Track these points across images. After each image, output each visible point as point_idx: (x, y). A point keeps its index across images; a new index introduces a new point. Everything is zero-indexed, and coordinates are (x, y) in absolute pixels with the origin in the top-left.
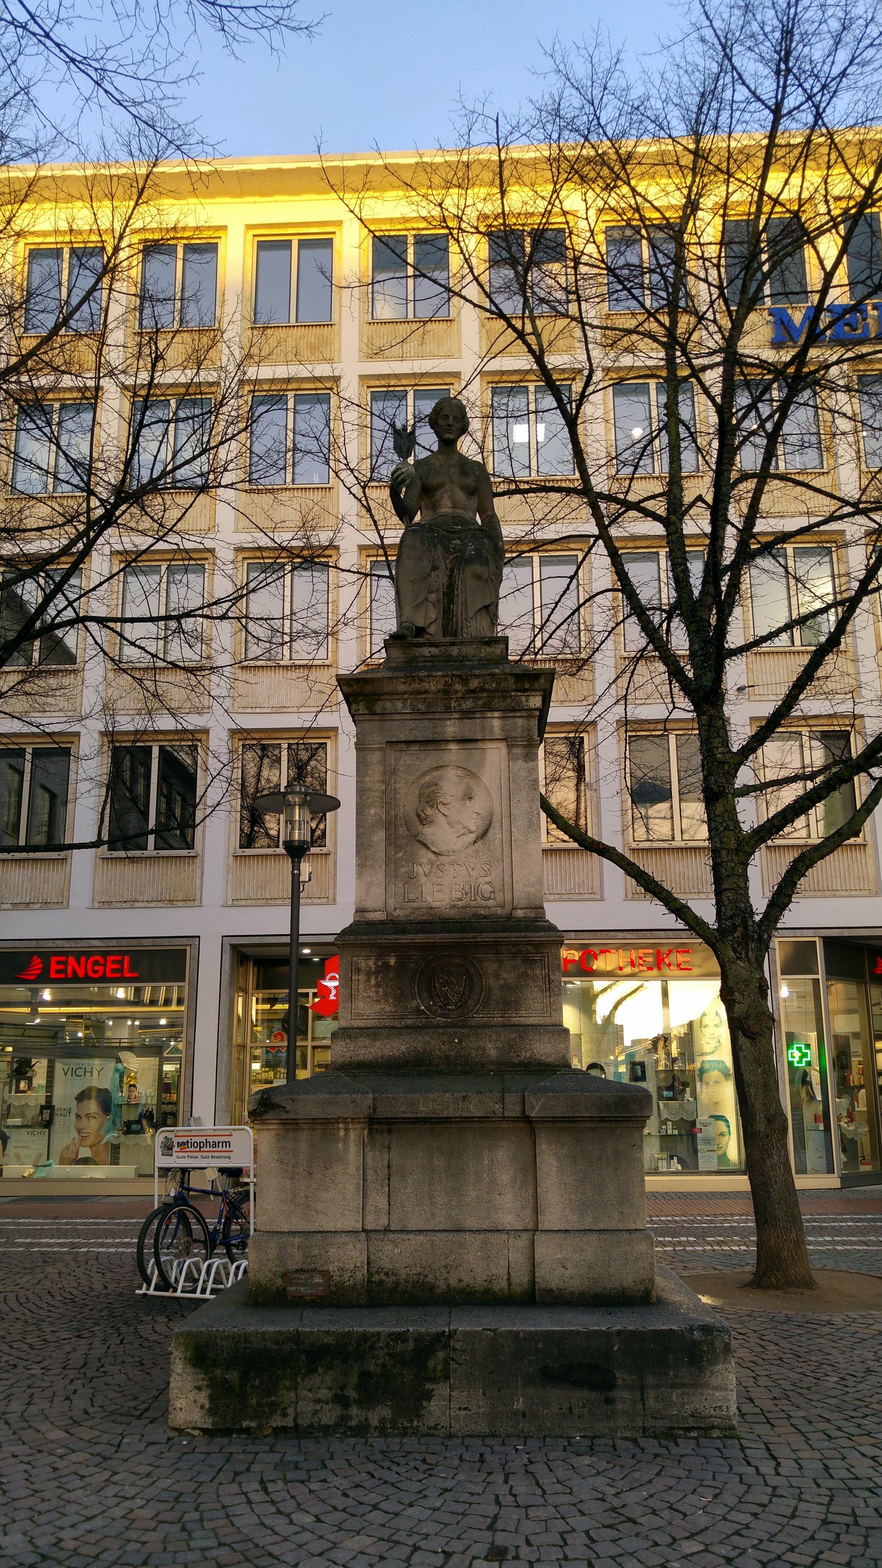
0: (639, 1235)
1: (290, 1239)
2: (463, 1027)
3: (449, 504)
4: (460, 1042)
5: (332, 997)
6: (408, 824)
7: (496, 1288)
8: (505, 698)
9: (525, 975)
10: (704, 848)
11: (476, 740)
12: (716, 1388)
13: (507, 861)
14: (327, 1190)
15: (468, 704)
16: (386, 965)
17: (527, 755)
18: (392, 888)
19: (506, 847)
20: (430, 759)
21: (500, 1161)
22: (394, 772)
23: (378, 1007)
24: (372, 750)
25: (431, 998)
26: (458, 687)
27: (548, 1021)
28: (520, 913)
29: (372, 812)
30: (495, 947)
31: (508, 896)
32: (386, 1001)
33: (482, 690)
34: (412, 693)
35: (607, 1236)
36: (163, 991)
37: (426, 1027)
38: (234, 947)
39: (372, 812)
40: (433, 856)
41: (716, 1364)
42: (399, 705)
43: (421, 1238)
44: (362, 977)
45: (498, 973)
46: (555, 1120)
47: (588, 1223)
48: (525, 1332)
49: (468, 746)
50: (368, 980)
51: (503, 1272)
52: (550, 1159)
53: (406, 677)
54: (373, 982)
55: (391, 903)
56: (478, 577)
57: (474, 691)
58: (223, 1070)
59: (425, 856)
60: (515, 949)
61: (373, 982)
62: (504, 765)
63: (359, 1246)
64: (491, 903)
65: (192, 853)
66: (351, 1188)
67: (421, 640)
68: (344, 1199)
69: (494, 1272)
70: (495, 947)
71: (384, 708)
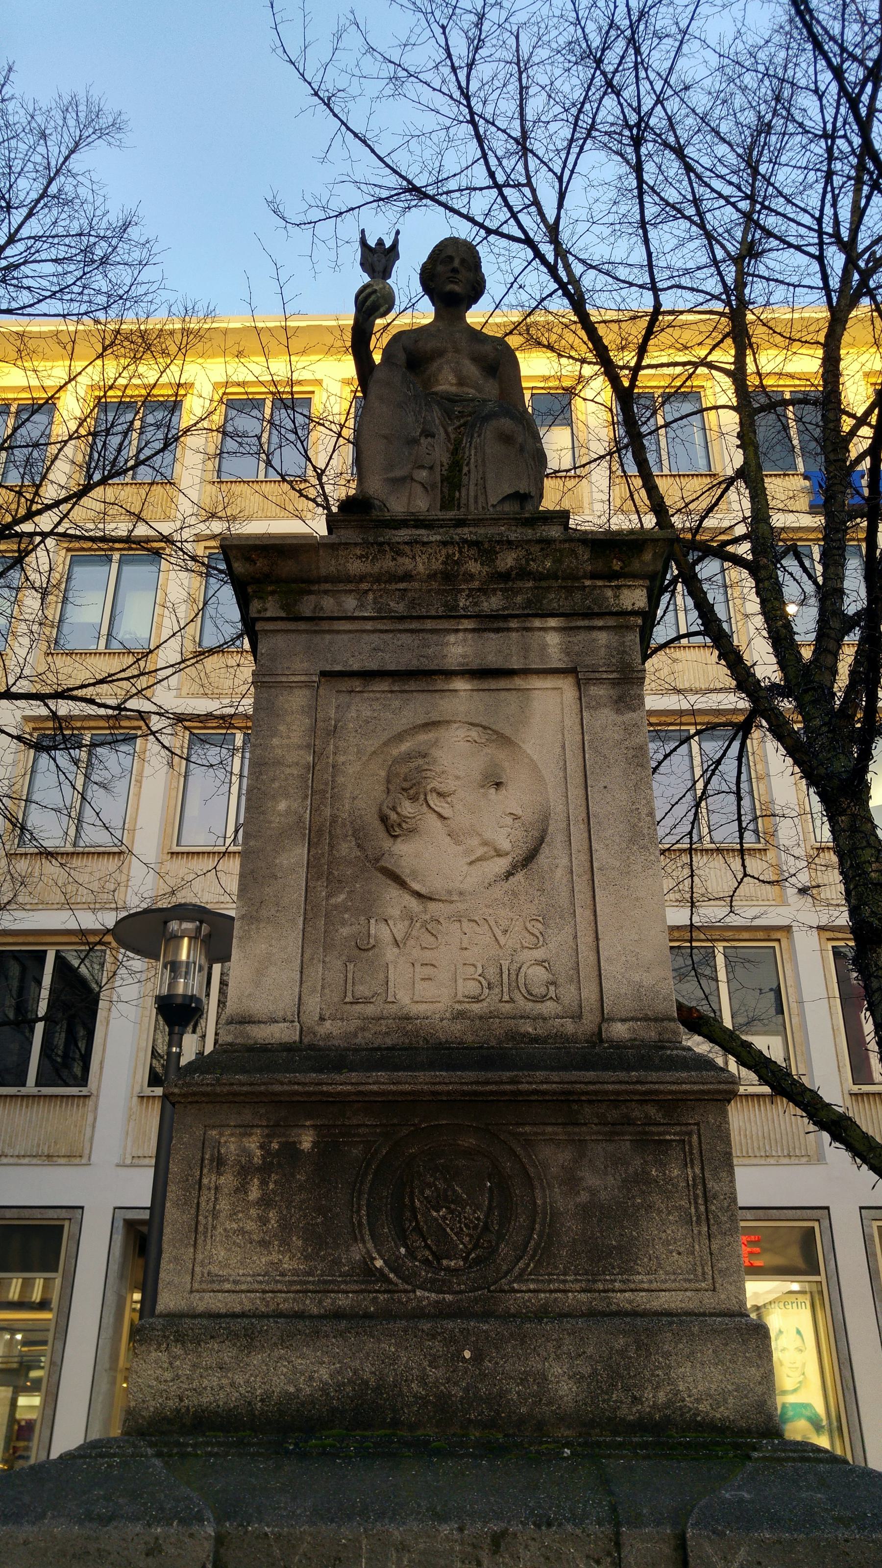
2: (486, 1316)
3: (452, 378)
4: (478, 1358)
6: (360, 836)
8: (570, 590)
9: (642, 1180)
11: (510, 673)
13: (583, 915)
15: (493, 603)
16: (291, 1150)
18: (316, 972)
19: (582, 885)
20: (412, 709)
22: (334, 732)
23: (261, 1261)
24: (290, 687)
25: (402, 1237)
26: (473, 567)
27: (709, 1301)
28: (619, 1030)
29: (282, 806)
30: (565, 1106)
31: (589, 993)
32: (285, 1243)
34: (377, 579)
36: (39, 1284)
37: (387, 1315)
39: (282, 806)
40: (414, 904)
42: (350, 603)
44: (228, 1180)
45: (573, 1176)
49: (493, 684)
50: (242, 1189)
53: (366, 544)
54: (254, 1194)
55: (313, 1005)
57: (505, 576)
58: (98, 1407)
59: (395, 901)
60: (614, 1115)
61: (254, 1194)
62: (571, 721)
64: (548, 1008)
65: (84, 1091)
70: (565, 1106)
71: (318, 607)
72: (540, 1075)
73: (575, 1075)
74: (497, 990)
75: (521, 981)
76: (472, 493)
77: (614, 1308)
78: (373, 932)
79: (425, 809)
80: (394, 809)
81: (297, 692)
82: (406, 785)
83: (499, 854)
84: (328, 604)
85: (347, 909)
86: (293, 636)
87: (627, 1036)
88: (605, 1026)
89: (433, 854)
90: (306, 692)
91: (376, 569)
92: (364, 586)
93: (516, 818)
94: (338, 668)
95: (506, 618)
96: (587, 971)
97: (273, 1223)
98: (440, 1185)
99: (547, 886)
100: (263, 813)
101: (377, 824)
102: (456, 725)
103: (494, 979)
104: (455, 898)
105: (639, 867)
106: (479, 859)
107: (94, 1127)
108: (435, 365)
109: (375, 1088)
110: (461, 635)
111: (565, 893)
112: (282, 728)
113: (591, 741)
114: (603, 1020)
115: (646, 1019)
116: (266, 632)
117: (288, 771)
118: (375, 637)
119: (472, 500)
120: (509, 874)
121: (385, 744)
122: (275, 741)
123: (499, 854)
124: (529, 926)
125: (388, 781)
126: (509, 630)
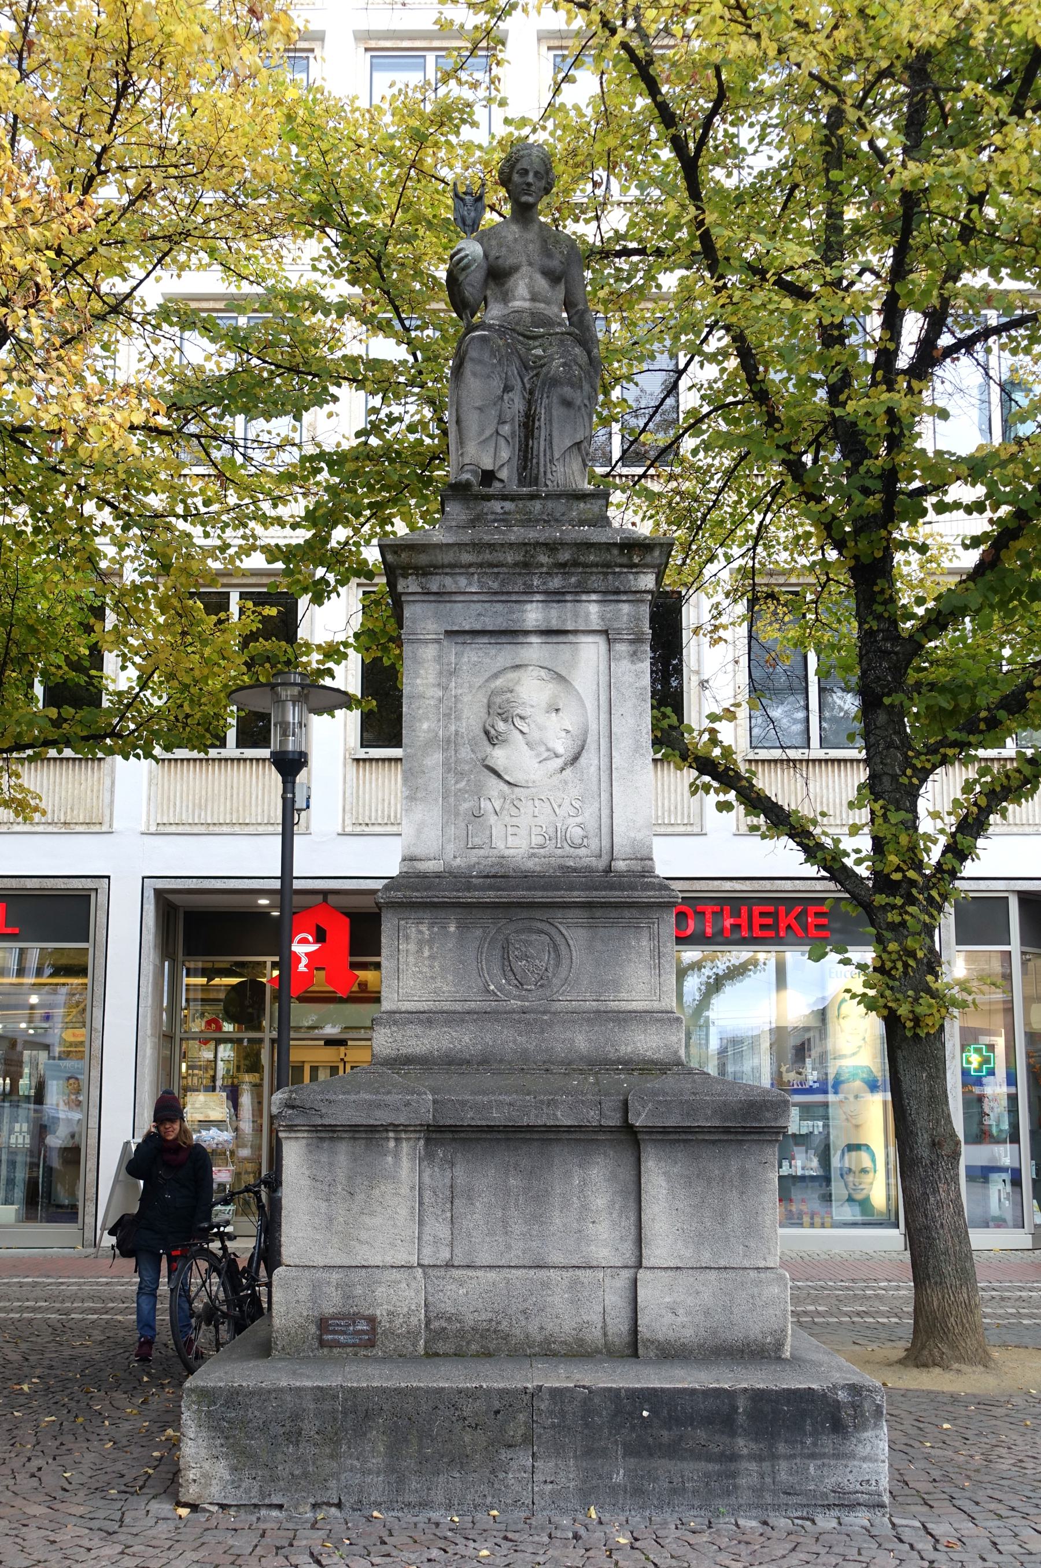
0: (769, 1274)
1: (325, 1275)
5: (302, 968)
7: (588, 1338)
10: (858, 761)
12: (864, 1459)
13: (605, 796)
14: (372, 1214)
15: (556, 583)
17: (635, 653)
19: (605, 777)
20: (503, 655)
21: (591, 1187)
24: (426, 642)
26: (543, 559)
27: (656, 1006)
28: (620, 865)
29: (425, 726)
31: (606, 843)
33: (576, 564)
34: (481, 565)
35: (731, 1274)
38: (159, 893)
39: (425, 726)
40: (505, 788)
41: (865, 1430)
42: (463, 581)
43: (492, 1275)
46: (665, 1130)
47: (706, 1258)
48: (628, 1390)
49: (555, 639)
50: (420, 951)
51: (596, 1319)
52: (658, 1177)
54: (426, 954)
56: (567, 404)
57: (564, 565)
61: (426, 954)
63: (414, 1285)
64: (583, 851)
66: (403, 1212)
67: (491, 491)
68: (395, 1226)
69: (586, 1318)
72: (576, 893)
83: (557, 756)
84: (449, 584)
89: (513, 757)
92: (472, 570)
95: (564, 593)
96: (605, 830)
107: (112, 792)
111: (595, 780)
118: (478, 606)
120: (563, 769)
123: (557, 756)
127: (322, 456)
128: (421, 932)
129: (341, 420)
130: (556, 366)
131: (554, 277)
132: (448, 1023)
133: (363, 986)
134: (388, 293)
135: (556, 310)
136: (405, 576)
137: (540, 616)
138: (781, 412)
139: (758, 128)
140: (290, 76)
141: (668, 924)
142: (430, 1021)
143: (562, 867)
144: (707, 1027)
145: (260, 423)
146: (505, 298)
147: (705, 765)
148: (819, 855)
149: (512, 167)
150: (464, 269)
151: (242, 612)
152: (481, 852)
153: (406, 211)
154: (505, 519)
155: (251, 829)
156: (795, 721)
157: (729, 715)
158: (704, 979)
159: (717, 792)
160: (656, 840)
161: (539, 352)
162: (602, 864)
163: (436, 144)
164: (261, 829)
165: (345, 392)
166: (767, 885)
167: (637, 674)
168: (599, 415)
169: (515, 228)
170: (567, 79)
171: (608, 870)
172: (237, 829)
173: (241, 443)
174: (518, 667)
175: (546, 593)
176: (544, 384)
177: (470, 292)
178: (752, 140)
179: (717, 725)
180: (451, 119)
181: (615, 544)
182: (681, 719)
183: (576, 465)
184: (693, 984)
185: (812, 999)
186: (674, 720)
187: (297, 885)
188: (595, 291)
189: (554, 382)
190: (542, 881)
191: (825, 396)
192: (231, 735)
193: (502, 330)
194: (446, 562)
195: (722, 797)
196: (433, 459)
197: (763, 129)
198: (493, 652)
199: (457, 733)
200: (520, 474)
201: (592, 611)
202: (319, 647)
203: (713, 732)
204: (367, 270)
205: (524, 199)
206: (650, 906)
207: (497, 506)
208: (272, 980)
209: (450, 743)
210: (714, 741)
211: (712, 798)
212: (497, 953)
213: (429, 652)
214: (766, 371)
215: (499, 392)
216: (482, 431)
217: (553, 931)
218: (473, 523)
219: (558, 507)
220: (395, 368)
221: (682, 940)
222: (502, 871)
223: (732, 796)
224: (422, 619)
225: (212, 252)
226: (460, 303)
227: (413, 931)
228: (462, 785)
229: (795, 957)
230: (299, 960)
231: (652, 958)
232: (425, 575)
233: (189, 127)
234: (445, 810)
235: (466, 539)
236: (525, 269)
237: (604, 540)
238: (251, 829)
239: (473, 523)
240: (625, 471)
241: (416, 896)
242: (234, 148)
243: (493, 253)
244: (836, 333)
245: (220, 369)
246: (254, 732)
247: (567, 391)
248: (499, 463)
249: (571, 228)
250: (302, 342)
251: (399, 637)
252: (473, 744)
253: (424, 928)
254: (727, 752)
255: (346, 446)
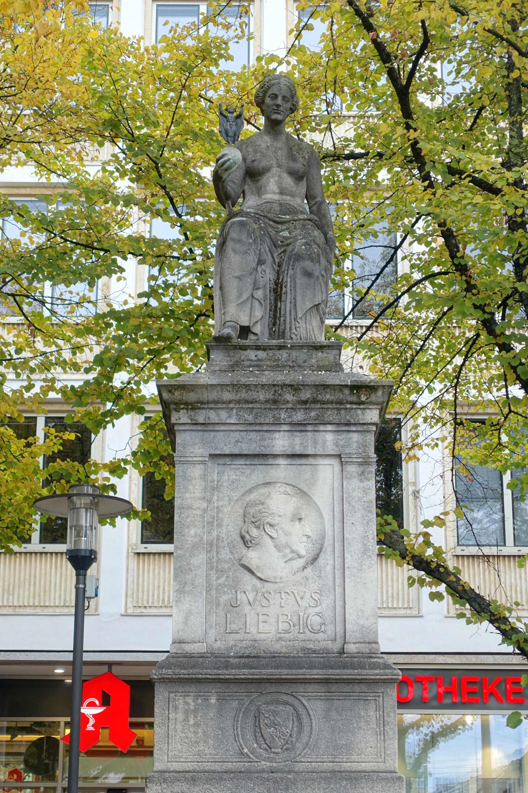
5: (90, 727)
13: (338, 590)
15: (299, 416)
17: (363, 473)
19: (338, 575)
20: (257, 474)
24: (193, 463)
26: (289, 397)
27: (381, 766)
28: (351, 648)
29: (193, 532)
31: (339, 629)
33: (315, 401)
34: (239, 402)
39: (193, 532)
40: (258, 583)
42: (224, 415)
49: (298, 461)
50: (186, 719)
54: (192, 722)
56: (308, 274)
57: (305, 402)
61: (192, 722)
64: (321, 636)
67: (247, 342)
72: (315, 671)
73: (331, 671)
74: (297, 627)
75: (309, 623)
76: (288, 310)
77: (342, 769)
78: (239, 598)
79: (263, 533)
80: (248, 532)
81: (197, 466)
82: (253, 520)
83: (300, 557)
84: (213, 416)
85: (226, 586)
86: (194, 433)
87: (356, 651)
88: (346, 646)
89: (266, 557)
90: (202, 466)
91: (238, 398)
92: (231, 405)
93: (308, 537)
94: (218, 452)
96: (339, 618)
97: (200, 734)
98: (272, 718)
99: (323, 574)
100: (183, 535)
101: (239, 539)
102: (279, 485)
103: (296, 622)
104: (278, 581)
105: (366, 567)
106: (290, 560)
108: (265, 178)
109: (243, 677)
110: (282, 433)
111: (330, 577)
112: (191, 487)
113: (347, 498)
114: (345, 643)
115: (365, 642)
116: (180, 431)
117: (195, 512)
118: (236, 434)
119: (288, 314)
120: (304, 568)
121: (243, 495)
122: (188, 495)
123: (300, 557)
124: (313, 595)
125: (245, 516)
126: (306, 431)
127: (113, 314)
128: (187, 703)
129: (127, 285)
130: (299, 246)
131: (298, 176)
132: (208, 781)
133: (141, 742)
134: (164, 188)
135: (299, 201)
136: (177, 410)
137: (286, 443)
138: (477, 281)
139: (455, 64)
140: (91, 21)
141: (392, 693)
142: (194, 780)
143: (303, 649)
144: (426, 779)
145: (61, 288)
146: (259, 192)
147: (420, 563)
148: (514, 637)
149: (265, 93)
150: (226, 170)
151: (46, 436)
152: (238, 636)
153: (178, 125)
154: (258, 365)
155: (50, 611)
156: (494, 521)
157: (439, 521)
158: (422, 736)
159: (430, 585)
160: (381, 622)
161: (286, 234)
162: (336, 647)
163: (201, 74)
164: (58, 611)
165: (130, 264)
166: (473, 659)
167: (365, 489)
168: (334, 282)
169: (267, 138)
170: (306, 27)
171: (342, 652)
172: (38, 611)
173: (49, 300)
174: (268, 483)
175: (290, 424)
176: (290, 259)
177: (231, 188)
178: (450, 73)
179: (429, 530)
180: (210, 53)
181: (346, 386)
182: (401, 526)
183: (315, 322)
184: (413, 739)
185: (511, 752)
186: (395, 525)
187: (86, 657)
188: (328, 186)
189: (298, 257)
190: (287, 661)
191: (512, 268)
192: (36, 536)
193: (257, 217)
194: (211, 399)
195: (434, 589)
196: (199, 316)
197: (459, 65)
198: (248, 472)
199: (218, 537)
200: (271, 329)
201: (328, 439)
202: (105, 466)
203: (426, 535)
204: (147, 169)
205: (274, 116)
206: (376, 682)
207: (252, 354)
208: (65, 738)
209: (212, 546)
210: (427, 543)
211: (426, 590)
212: (250, 721)
213: (196, 471)
214: (464, 249)
215: (254, 265)
216: (240, 296)
217: (296, 703)
218: (233, 367)
219: (301, 355)
220: (170, 246)
221: (403, 703)
222: (254, 652)
223: (442, 588)
224: (191, 446)
225: (28, 153)
226: (224, 197)
227: (180, 703)
228: (222, 580)
229: (497, 719)
230: (87, 720)
231: (378, 725)
232: (193, 409)
233: (11, 59)
234: (208, 602)
235: (227, 381)
236: (275, 170)
237: (337, 382)
238: (50, 611)
239: (233, 367)
240: (354, 323)
241: (183, 673)
242: (46, 74)
243: (250, 158)
244: (519, 220)
245: (32, 243)
246: (54, 532)
247: (308, 265)
248: (254, 320)
249: (311, 137)
250: (96, 225)
251: (172, 457)
252: (232, 546)
253: (190, 700)
254: (438, 552)
255: (131, 305)
